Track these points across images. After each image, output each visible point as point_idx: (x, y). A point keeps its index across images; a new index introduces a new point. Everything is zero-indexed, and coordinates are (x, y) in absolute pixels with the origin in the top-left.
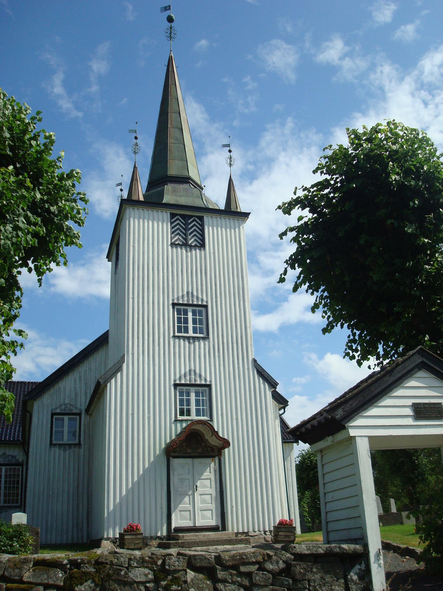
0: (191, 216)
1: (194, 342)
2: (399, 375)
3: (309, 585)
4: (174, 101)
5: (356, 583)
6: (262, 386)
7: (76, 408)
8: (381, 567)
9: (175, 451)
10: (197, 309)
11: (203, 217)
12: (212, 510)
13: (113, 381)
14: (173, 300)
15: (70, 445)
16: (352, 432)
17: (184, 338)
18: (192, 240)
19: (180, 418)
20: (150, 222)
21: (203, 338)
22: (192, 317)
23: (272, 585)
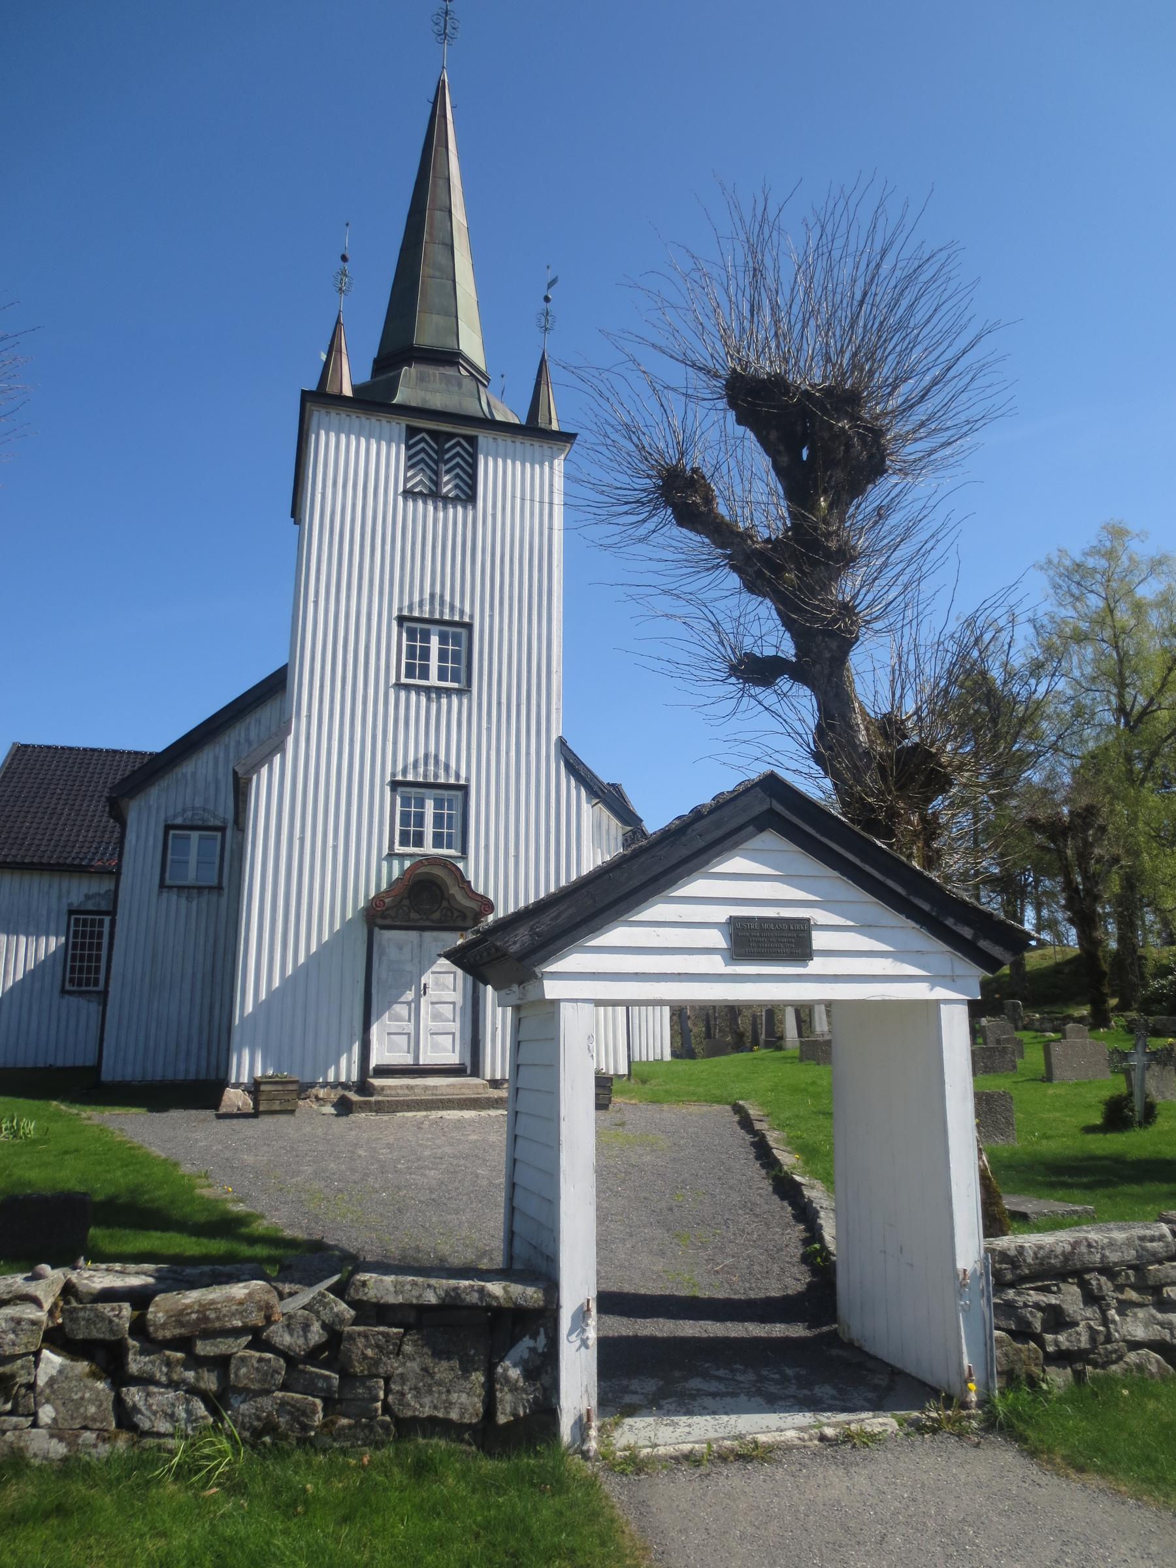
0: (451, 436)
1: (439, 698)
2: (701, 843)
3: (387, 1391)
4: (441, 182)
5: (514, 1389)
6: (574, 792)
7: (215, 816)
8: (587, 1347)
9: (379, 916)
10: (450, 629)
11: (476, 437)
12: (454, 1034)
13: (264, 770)
14: (400, 609)
15: (200, 889)
16: (552, 990)
17: (419, 689)
18: (450, 486)
19: (398, 849)
20: (500, 461)
21: (459, 692)
22: (438, 648)
23: (284, 1387)
